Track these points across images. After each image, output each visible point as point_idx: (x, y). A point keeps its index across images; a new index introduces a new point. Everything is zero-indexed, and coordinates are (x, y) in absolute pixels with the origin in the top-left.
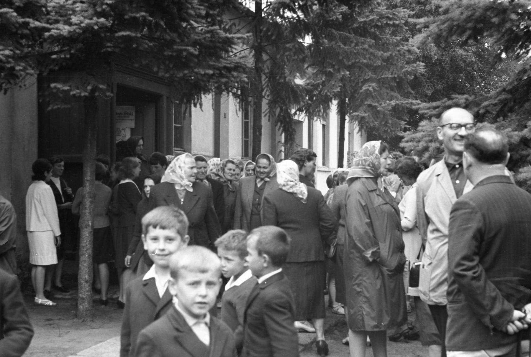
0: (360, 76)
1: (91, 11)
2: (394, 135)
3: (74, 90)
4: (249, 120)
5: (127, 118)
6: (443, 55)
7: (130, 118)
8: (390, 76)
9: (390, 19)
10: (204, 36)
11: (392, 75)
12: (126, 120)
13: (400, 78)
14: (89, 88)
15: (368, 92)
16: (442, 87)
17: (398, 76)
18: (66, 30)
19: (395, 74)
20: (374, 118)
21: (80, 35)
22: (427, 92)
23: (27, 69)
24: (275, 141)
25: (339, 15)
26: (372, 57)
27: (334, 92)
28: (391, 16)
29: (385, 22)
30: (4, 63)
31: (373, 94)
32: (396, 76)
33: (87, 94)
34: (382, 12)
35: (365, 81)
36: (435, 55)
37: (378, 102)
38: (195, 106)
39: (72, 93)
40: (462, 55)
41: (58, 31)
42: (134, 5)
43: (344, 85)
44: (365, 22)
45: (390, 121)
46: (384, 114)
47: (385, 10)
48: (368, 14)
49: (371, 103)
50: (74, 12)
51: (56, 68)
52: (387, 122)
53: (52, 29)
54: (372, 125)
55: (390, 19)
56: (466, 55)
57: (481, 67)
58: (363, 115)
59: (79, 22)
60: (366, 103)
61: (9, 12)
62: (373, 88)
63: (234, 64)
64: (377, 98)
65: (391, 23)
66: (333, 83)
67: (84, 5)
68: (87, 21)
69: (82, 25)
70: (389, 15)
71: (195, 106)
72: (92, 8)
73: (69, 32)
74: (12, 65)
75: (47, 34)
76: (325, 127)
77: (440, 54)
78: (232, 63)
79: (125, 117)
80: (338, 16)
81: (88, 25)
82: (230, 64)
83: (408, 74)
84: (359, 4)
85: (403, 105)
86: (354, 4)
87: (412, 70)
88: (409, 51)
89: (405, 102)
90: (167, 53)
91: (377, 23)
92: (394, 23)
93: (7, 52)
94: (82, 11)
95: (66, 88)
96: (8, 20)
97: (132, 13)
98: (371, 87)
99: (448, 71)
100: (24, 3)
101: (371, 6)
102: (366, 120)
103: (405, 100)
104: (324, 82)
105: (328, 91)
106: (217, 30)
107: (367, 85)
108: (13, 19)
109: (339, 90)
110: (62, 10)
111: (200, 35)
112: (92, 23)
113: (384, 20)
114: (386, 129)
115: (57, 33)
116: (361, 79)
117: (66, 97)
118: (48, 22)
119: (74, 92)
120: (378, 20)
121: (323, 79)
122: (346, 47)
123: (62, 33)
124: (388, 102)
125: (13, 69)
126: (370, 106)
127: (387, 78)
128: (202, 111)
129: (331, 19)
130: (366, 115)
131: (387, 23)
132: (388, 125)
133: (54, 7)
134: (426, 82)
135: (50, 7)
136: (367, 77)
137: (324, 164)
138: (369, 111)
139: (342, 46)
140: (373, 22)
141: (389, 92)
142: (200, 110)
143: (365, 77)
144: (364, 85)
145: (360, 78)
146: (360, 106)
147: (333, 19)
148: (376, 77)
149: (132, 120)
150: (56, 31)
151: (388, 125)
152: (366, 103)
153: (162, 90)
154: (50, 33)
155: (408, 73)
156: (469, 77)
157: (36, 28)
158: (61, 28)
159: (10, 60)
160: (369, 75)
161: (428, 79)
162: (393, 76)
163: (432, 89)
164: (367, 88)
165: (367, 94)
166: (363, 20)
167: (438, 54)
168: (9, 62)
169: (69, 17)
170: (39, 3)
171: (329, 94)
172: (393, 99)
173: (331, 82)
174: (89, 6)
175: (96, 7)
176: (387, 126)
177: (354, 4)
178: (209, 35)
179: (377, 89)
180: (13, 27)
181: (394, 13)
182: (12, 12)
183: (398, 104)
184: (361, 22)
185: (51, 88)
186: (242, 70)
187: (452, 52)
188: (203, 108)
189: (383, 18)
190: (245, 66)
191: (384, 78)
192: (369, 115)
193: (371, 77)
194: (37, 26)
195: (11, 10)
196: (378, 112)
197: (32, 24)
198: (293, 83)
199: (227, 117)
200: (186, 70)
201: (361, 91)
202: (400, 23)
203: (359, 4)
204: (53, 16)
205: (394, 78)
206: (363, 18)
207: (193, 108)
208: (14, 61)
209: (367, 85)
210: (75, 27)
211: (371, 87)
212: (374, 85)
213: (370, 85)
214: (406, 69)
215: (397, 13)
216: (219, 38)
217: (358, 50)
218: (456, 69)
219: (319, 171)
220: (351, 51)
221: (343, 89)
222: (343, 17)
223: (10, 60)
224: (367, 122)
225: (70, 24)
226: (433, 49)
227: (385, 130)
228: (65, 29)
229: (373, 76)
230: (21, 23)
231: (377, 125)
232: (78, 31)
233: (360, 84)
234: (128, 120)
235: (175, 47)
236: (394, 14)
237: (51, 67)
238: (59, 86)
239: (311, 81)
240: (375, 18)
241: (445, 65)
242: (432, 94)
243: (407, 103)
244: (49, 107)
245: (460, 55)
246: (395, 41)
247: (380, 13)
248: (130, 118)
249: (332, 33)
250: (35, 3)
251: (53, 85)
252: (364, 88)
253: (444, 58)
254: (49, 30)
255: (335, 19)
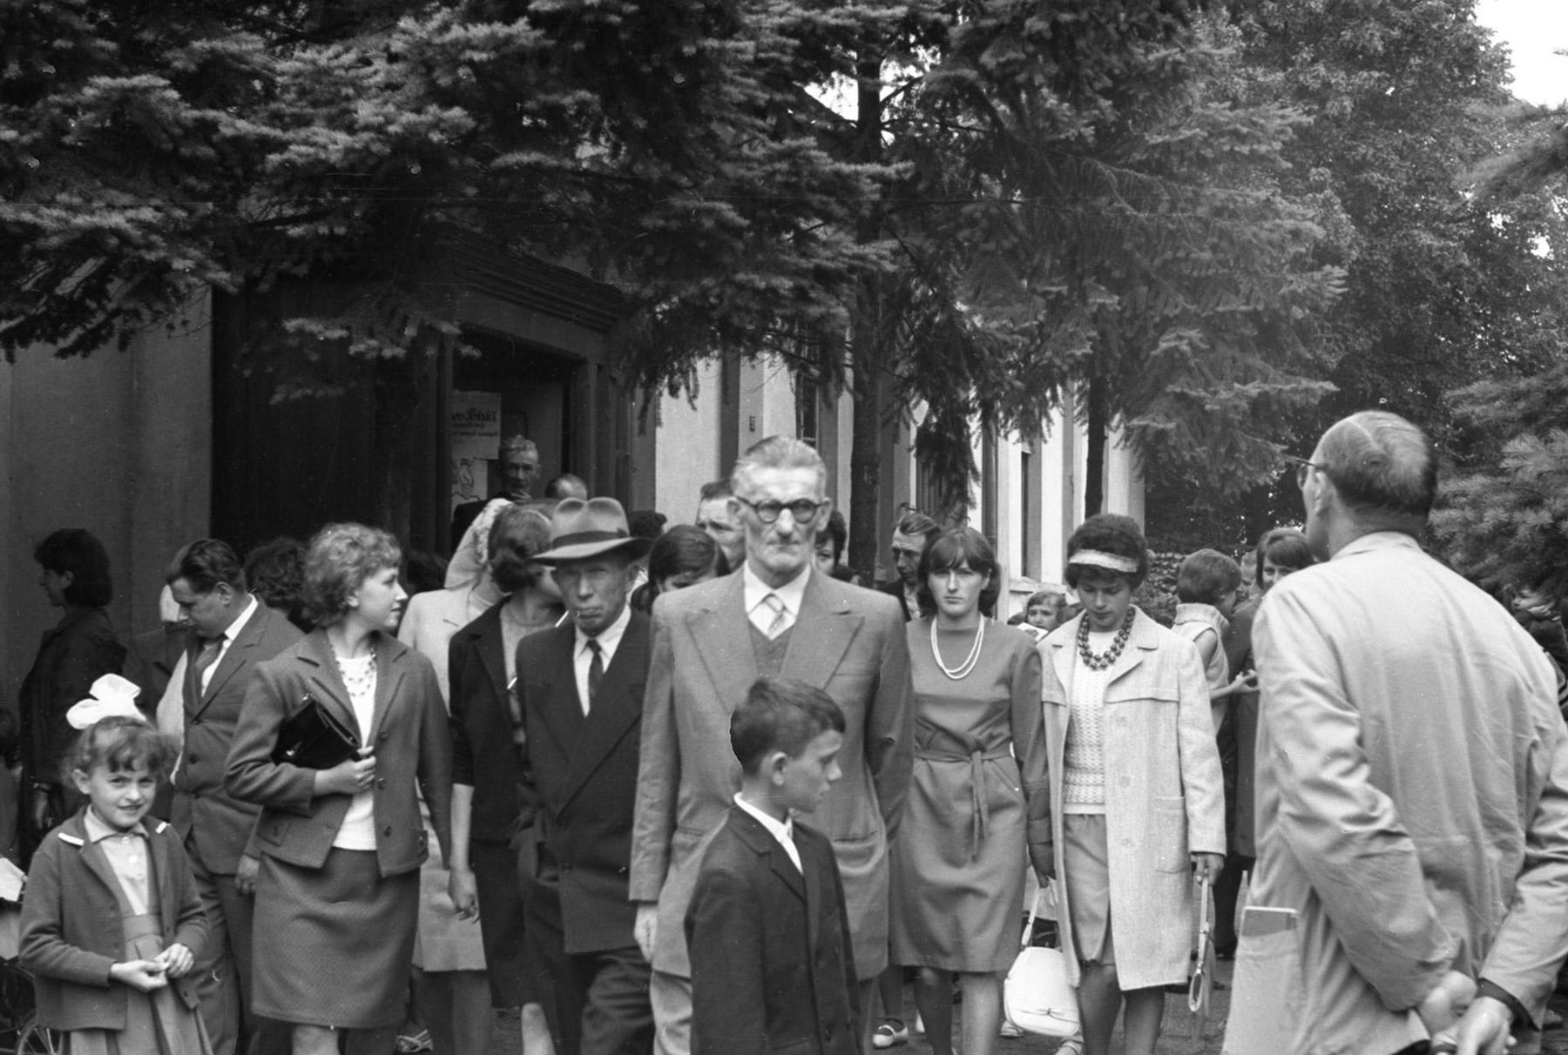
0: (1151, 308)
1: (414, 87)
2: (1250, 484)
3: (360, 341)
4: (817, 439)
5: (478, 430)
6: (1373, 247)
7: (486, 430)
8: (1243, 308)
9: (1240, 138)
10: (768, 168)
11: (1247, 303)
12: (474, 434)
13: (1275, 315)
14: (410, 332)
15: (1177, 356)
16: (1370, 343)
17: (1266, 308)
18: (340, 147)
19: (1257, 301)
20: (1195, 436)
21: (381, 159)
22: (1325, 357)
23: (207, 269)
24: (892, 500)
25: (1087, 126)
26: (1224, 244)
27: (1072, 356)
28: (1245, 130)
29: (1227, 148)
30: (137, 247)
31: (1192, 363)
32: (1260, 308)
33: (400, 352)
34: (1217, 116)
35: (1165, 325)
36: (1350, 247)
37: (1207, 385)
38: (674, 392)
39: (353, 350)
40: (1430, 247)
41: (311, 150)
42: (554, 70)
43: (1102, 334)
44: (1166, 147)
45: (1243, 446)
46: (1227, 424)
47: (1228, 112)
48: (1173, 122)
49: (1186, 390)
50: (361, 92)
51: (302, 270)
52: (1233, 449)
53: (289, 143)
54: (1188, 458)
55: (1240, 138)
56: (1441, 249)
57: (1484, 284)
58: (1161, 426)
59: (381, 119)
60: (1170, 388)
61: (154, 88)
62: (1191, 344)
63: (846, 260)
64: (1202, 374)
65: (1245, 149)
66: (1071, 330)
67: (398, 67)
68: (408, 117)
69: (392, 129)
70: (1238, 126)
71: (674, 392)
72: (421, 74)
73: (349, 151)
74: (162, 254)
75: (274, 158)
76: (1029, 462)
77: (1365, 244)
78: (841, 258)
79: (470, 425)
80: (1082, 130)
81: (411, 129)
82: (833, 259)
83: (1293, 302)
84: (1147, 94)
85: (1284, 396)
86: (1131, 92)
87: (1309, 289)
88: (1296, 234)
89: (1288, 387)
90: (651, 221)
91: (1202, 152)
92: (1252, 151)
93: (147, 214)
94: (391, 86)
95: (337, 334)
96: (150, 112)
97: (547, 92)
98: (1185, 341)
99: (1387, 294)
100: (201, 61)
101: (1181, 98)
102: (1171, 443)
103: (1288, 382)
104: (1041, 326)
105: (1057, 354)
106: (809, 149)
107: (1174, 335)
108: (166, 109)
109: (1087, 350)
110: (320, 83)
111: (756, 165)
112: (422, 123)
113: (1222, 140)
114: (1232, 468)
115: (308, 155)
116: (1153, 317)
117: (335, 356)
118: (276, 119)
119: (361, 347)
120: (1206, 142)
121: (1041, 318)
122: (1143, 215)
123: (323, 155)
124: (1237, 385)
125: (163, 267)
126: (1181, 397)
127: (1232, 313)
128: (694, 408)
129: (1062, 136)
130: (1171, 426)
131: (1232, 150)
132: (1237, 455)
133: (297, 75)
134: (1322, 327)
135: (282, 74)
136: (1171, 312)
137: (1025, 573)
138: (1178, 413)
139: (1130, 211)
140: (1191, 147)
141: (1238, 355)
142: (689, 407)
143: (1166, 312)
144: (1162, 333)
145: (1152, 313)
146: (1152, 399)
147: (1068, 138)
148: (1199, 311)
149: (491, 435)
150: (303, 149)
151: (1237, 455)
152: (1170, 388)
153: (588, 347)
154: (286, 156)
155: (1295, 299)
156: (1448, 313)
157: (238, 141)
158: (321, 140)
159: (154, 238)
160: (1176, 306)
161: (1329, 321)
162: (1250, 308)
163: (1340, 348)
164: (1172, 344)
165: (1174, 363)
166: (1160, 140)
167: (1358, 244)
168: (150, 247)
169: (344, 105)
170: (247, 63)
171: (1058, 362)
172: (1254, 379)
173: (1063, 326)
174: (413, 71)
175: (436, 74)
176: (1233, 458)
177: (1131, 92)
178: (783, 166)
179: (1203, 346)
180: (164, 136)
181: (1255, 119)
182: (165, 88)
183: (1266, 393)
184: (1155, 147)
185: (285, 333)
186: (1515, 182)
187: (1401, 239)
188: (697, 402)
189: (1222, 134)
190: (875, 269)
191: (1222, 315)
192: (1178, 427)
193: (1185, 311)
194: (243, 131)
195: (162, 82)
196: (1208, 415)
197: (226, 125)
198: (968, 326)
199: (757, 424)
200: (707, 276)
201: (1153, 353)
202: (1268, 151)
203: (1147, 94)
204: (286, 104)
205: (1253, 316)
206: (1159, 134)
207: (666, 401)
208: (165, 241)
209: (1174, 335)
210: (366, 136)
211: (1185, 341)
212: (1194, 334)
213: (1183, 334)
214: (1292, 287)
215: (1262, 121)
216: (813, 174)
217: (1181, 223)
218: (1412, 291)
219: (1013, 592)
220: (1159, 227)
221: (1101, 348)
222: (1097, 134)
223: (154, 238)
224: (1174, 448)
225: (351, 129)
226: (1345, 229)
227: (1226, 469)
228: (334, 143)
229: (1189, 307)
230: (189, 124)
231: (1204, 456)
232: (375, 148)
233: (1152, 333)
234: (480, 434)
235: (677, 202)
236: (1254, 124)
237: (286, 265)
238: (313, 326)
239: (1004, 322)
240: (1196, 135)
241: (1379, 277)
242: (1340, 364)
243: (1295, 391)
244: (275, 393)
245: (1425, 249)
246: (1252, 202)
247: (1211, 121)
248: (486, 430)
249: (1096, 173)
250: (235, 65)
251: (291, 325)
252: (1163, 345)
253: (1376, 258)
254: (282, 146)
255: (1073, 139)
